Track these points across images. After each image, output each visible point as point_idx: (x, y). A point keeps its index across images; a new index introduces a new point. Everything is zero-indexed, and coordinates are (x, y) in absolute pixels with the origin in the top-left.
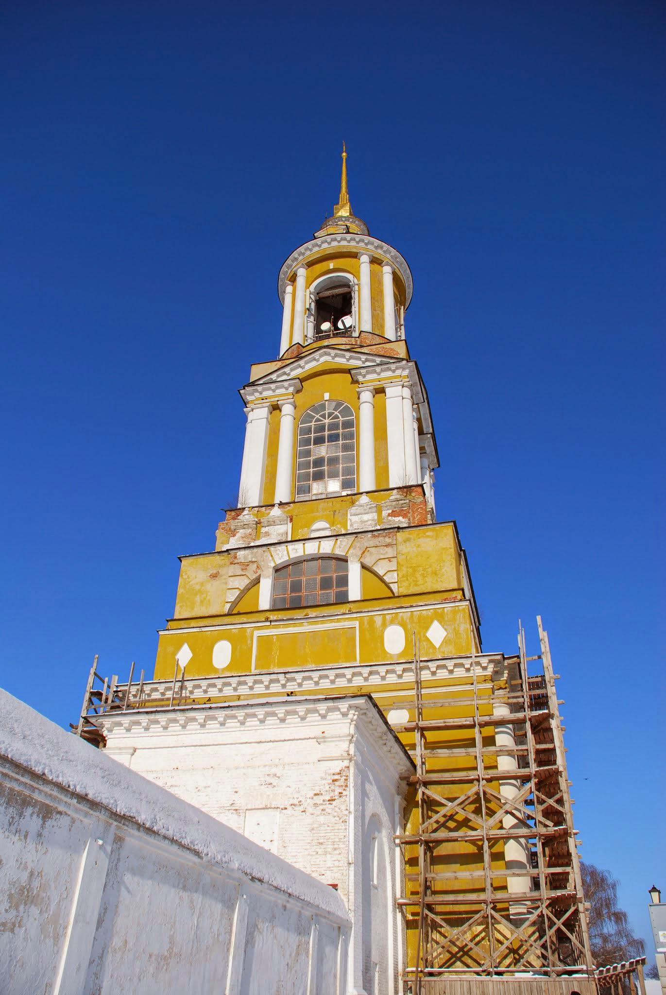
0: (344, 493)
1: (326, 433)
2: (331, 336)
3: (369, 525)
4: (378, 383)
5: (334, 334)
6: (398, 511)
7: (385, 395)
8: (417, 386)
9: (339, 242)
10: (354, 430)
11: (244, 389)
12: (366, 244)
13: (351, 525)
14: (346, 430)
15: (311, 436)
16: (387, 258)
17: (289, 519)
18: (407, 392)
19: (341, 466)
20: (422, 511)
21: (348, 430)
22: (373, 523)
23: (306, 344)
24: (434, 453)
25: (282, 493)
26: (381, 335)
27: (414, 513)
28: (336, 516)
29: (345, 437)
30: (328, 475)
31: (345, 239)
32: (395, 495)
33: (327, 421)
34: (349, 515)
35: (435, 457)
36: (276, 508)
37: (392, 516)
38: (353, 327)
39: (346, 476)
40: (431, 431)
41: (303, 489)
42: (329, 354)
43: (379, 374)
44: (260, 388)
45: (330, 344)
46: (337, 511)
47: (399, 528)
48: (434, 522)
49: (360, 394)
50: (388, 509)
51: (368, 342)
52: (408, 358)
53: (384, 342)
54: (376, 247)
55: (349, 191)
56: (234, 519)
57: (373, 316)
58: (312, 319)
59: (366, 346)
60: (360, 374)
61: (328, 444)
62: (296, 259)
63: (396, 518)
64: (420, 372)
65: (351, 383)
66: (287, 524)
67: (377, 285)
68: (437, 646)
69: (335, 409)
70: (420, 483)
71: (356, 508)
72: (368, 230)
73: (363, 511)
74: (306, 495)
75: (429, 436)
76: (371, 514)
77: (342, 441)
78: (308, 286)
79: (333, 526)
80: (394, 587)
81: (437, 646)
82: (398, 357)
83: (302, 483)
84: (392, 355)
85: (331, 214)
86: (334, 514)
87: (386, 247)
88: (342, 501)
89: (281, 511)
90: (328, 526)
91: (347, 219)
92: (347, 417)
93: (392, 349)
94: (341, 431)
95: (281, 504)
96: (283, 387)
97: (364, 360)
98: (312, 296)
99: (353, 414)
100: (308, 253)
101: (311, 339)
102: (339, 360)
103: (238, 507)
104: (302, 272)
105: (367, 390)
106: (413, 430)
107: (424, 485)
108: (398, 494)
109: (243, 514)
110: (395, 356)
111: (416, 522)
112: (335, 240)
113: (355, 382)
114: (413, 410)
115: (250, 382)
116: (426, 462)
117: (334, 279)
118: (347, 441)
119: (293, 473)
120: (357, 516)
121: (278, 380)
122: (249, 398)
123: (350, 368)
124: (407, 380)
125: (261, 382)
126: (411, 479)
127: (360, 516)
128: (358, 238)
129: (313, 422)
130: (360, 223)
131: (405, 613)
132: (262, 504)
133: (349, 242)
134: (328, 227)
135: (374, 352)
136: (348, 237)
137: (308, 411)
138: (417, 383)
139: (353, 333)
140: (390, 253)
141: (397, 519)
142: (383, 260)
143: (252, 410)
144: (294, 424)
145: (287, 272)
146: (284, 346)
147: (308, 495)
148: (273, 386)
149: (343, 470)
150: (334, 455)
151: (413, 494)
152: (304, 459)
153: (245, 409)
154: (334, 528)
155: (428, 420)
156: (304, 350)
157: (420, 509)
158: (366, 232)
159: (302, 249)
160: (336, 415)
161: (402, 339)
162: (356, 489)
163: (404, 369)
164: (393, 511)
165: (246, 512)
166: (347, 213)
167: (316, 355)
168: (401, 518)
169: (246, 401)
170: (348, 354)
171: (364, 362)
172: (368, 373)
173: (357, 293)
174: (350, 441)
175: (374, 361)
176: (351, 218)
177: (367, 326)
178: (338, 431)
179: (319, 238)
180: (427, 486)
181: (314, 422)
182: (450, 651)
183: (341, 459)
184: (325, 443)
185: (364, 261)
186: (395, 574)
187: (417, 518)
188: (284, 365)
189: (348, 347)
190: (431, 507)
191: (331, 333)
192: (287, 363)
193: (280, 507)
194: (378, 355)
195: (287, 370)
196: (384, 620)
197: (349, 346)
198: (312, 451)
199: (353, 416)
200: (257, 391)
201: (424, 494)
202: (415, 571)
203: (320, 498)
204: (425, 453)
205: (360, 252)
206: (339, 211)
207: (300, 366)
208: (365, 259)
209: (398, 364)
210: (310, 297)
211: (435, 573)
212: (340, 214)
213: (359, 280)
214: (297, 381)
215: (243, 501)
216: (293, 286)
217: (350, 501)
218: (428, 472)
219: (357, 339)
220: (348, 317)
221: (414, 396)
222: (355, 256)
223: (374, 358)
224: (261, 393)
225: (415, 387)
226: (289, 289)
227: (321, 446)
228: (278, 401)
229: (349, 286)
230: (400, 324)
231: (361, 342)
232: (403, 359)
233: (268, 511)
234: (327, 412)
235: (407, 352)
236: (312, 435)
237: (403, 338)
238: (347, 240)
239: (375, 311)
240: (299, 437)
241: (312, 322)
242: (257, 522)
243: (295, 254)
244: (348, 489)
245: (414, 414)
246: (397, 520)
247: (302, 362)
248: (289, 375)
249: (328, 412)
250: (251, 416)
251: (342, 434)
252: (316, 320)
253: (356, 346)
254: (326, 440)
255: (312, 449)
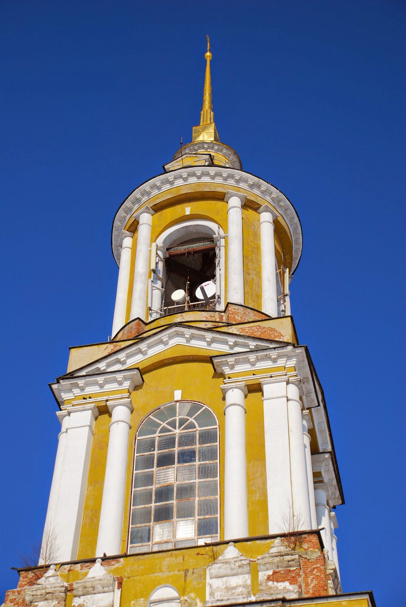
0: (201, 542)
1: (176, 449)
2: (186, 309)
3: (239, 595)
4: (252, 377)
5: (189, 307)
6: (282, 572)
7: (263, 395)
8: (308, 382)
9: (199, 178)
10: (217, 463)
11: (58, 382)
12: (238, 181)
13: (212, 594)
14: (206, 445)
15: (154, 454)
16: (265, 201)
17: (117, 583)
18: (293, 391)
19: (197, 499)
20: (319, 574)
21: (208, 445)
22: (245, 590)
23: (150, 319)
24: (335, 482)
26: (256, 308)
27: (306, 576)
28: (189, 579)
29: (204, 456)
30: (178, 512)
31: (208, 174)
32: (277, 546)
33: (177, 431)
34: (208, 577)
35: (337, 488)
36: (98, 564)
37: (273, 581)
38: (217, 297)
39: (204, 515)
40: (330, 449)
41: (139, 534)
42: (182, 335)
43: (253, 365)
44: (81, 382)
45: (184, 321)
46: (191, 571)
47: (284, 600)
48: (339, 593)
49: (226, 393)
50: (267, 569)
51: (239, 319)
52: (295, 342)
53: (260, 319)
54: (251, 186)
55: (214, 108)
56: (31, 583)
57: (246, 282)
58: (159, 284)
59: (235, 325)
60: (227, 364)
61: (178, 465)
62: (138, 200)
63: (280, 584)
64: (312, 363)
65: (213, 377)
66: (113, 591)
67: (251, 239)
69: (190, 414)
70: (314, 528)
71: (218, 565)
72: (240, 162)
73: (229, 572)
74: (144, 544)
75: (327, 456)
76: (242, 576)
77: (199, 461)
78: (154, 238)
79: (184, 595)
82: (281, 340)
83: (139, 525)
84: (272, 337)
85: (189, 139)
86: (186, 576)
87: (265, 185)
88: (198, 554)
89: (105, 570)
90: (175, 594)
91: (211, 145)
92: (207, 426)
93: (272, 329)
95: (105, 559)
96: (115, 380)
97: (232, 344)
98: (160, 253)
99: (216, 422)
100: (155, 192)
101: (157, 312)
102: (195, 343)
103: (39, 564)
104: (146, 219)
105: (236, 388)
106: (303, 448)
107: (321, 532)
108: (282, 546)
109: (47, 575)
110: (277, 339)
111: (311, 591)
112: (194, 175)
113: (219, 375)
114: (303, 417)
115: (68, 372)
116: (323, 496)
117: (191, 229)
118: (207, 462)
119: (125, 509)
120: (220, 579)
121: (109, 370)
122: (65, 396)
123: (212, 355)
124: (294, 373)
125: (83, 373)
126: (301, 522)
127: (224, 579)
128: (225, 172)
129: (158, 432)
130: (229, 153)
132: (76, 559)
133: (213, 178)
134: (183, 157)
135: (247, 332)
136: (212, 170)
137: (150, 416)
138: (308, 378)
139: (217, 305)
140: (271, 194)
141: (281, 585)
142: (261, 204)
143: (69, 414)
144: (129, 435)
145: (125, 217)
146: (118, 322)
147: (146, 543)
148: (100, 379)
149: (199, 505)
150: (187, 482)
151: (305, 546)
152: (143, 488)
153: (58, 413)
154: (186, 598)
155: (326, 433)
156: (147, 328)
157: (316, 570)
158: (237, 165)
159: (146, 186)
160: (191, 422)
161: (287, 315)
162: (219, 535)
163: (289, 357)
164: (275, 573)
165: (51, 572)
166: (210, 137)
167: (164, 336)
168: (287, 584)
169: (59, 400)
170: (209, 336)
171: (231, 347)
172: (237, 362)
173: (223, 250)
174: (211, 462)
175: (247, 346)
176: (217, 145)
177: (236, 297)
178: (194, 447)
179: (172, 171)
180: (326, 534)
181: (159, 433)
183: (197, 488)
184: (174, 464)
185: (234, 205)
187: (312, 585)
188: (118, 348)
189: (210, 325)
190: (333, 567)
191: (186, 305)
192: (123, 347)
193: (104, 563)
194: (253, 337)
195: (121, 356)
197: (212, 323)
198: (154, 477)
199: (216, 424)
200: (77, 386)
201: (322, 547)
203: (165, 549)
204: (322, 482)
205: (228, 193)
206: (199, 136)
207: (140, 352)
208: (235, 202)
209: (281, 351)
210: (157, 254)
212: (200, 138)
213: (226, 230)
214: (136, 372)
215: (48, 554)
216: (132, 237)
217: (211, 554)
218: (326, 512)
219: (223, 314)
220: (210, 282)
221: (304, 397)
222: (221, 197)
223: (246, 341)
224: (82, 389)
225: (306, 384)
226: (127, 242)
227: (168, 468)
228: (107, 401)
229: (211, 240)
230: (284, 293)
231: (228, 319)
232: (288, 344)
233: (85, 570)
234: (177, 418)
235: (293, 334)
236: (156, 452)
237: (288, 313)
238: (210, 176)
239: (249, 274)
240: (136, 455)
241: (158, 289)
242: (66, 588)
243: (137, 193)
244: (207, 536)
245: (305, 423)
246: (282, 588)
247: (143, 346)
248: (124, 363)
249: (179, 419)
250: (66, 423)
251: (199, 451)
252: (164, 285)
253: (221, 324)
254: (176, 460)
255: (155, 473)
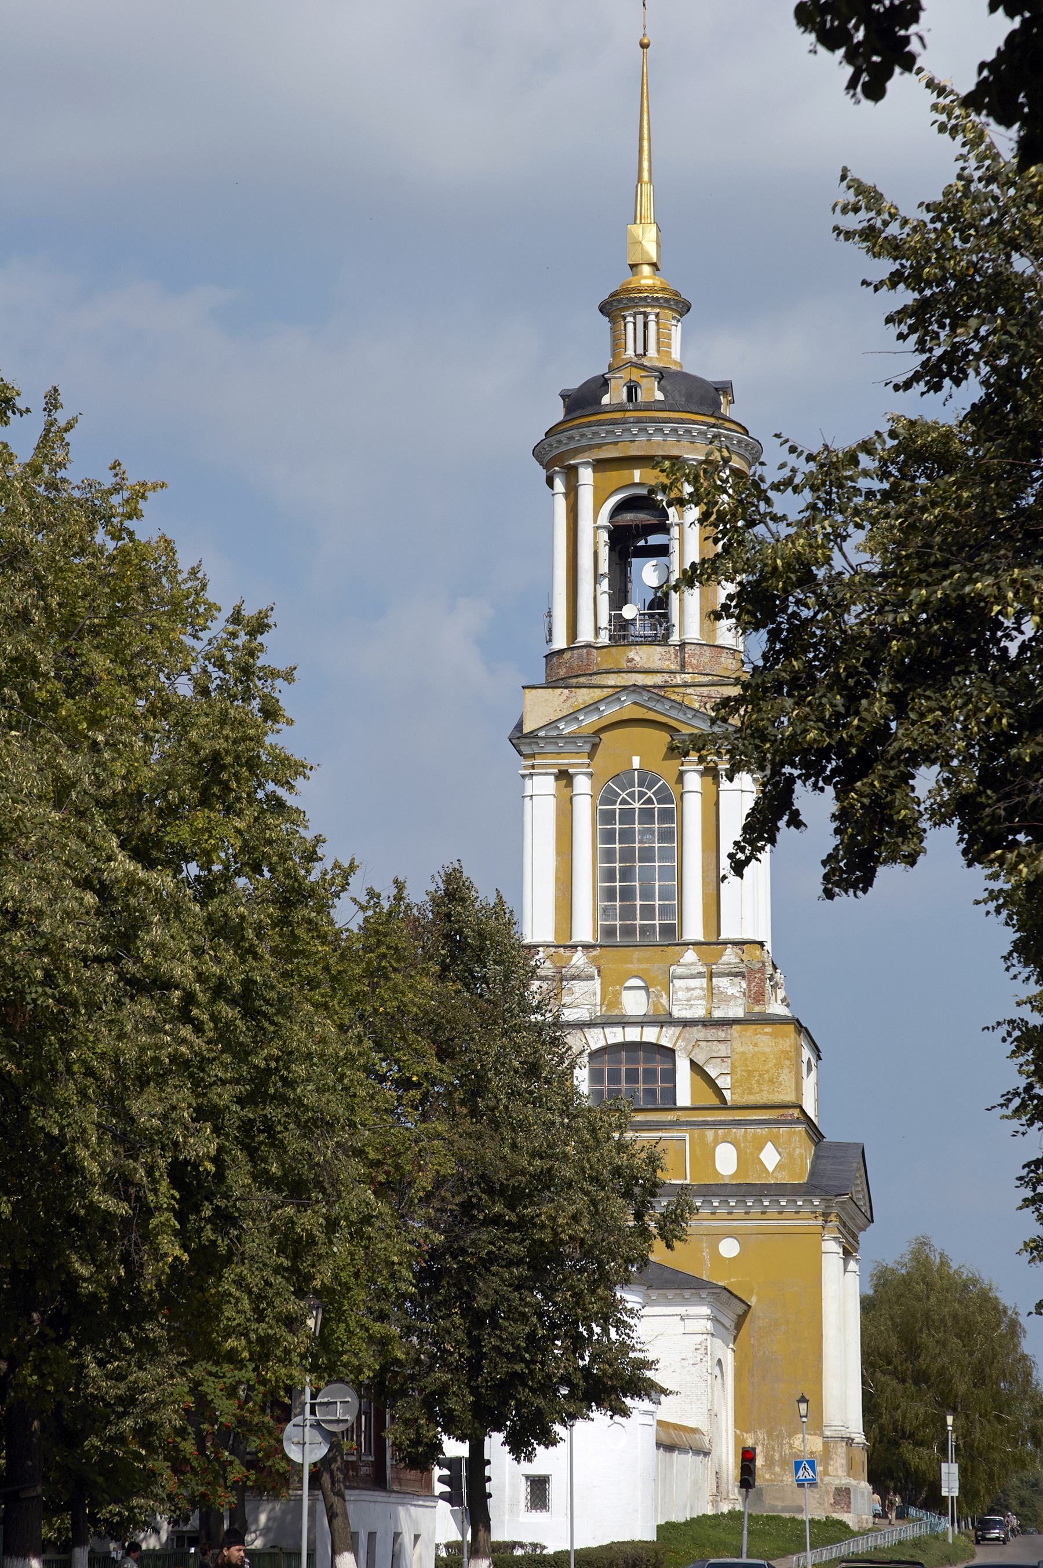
25: (584, 931)
33: (637, 805)
68: (771, 1170)
80: (727, 1094)
81: (771, 1170)
94: (657, 825)
95: (586, 947)
131: (739, 1132)
182: (784, 1178)
186: (729, 1078)
196: (716, 1135)
202: (750, 1074)
211: (772, 1081)
